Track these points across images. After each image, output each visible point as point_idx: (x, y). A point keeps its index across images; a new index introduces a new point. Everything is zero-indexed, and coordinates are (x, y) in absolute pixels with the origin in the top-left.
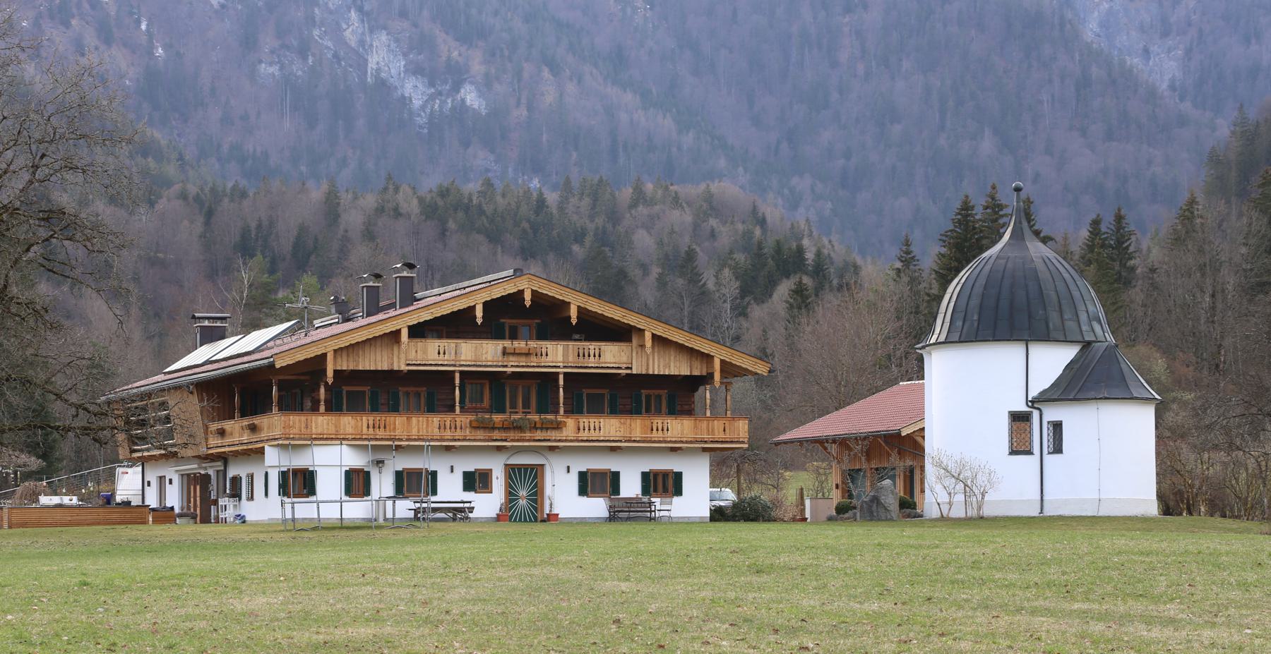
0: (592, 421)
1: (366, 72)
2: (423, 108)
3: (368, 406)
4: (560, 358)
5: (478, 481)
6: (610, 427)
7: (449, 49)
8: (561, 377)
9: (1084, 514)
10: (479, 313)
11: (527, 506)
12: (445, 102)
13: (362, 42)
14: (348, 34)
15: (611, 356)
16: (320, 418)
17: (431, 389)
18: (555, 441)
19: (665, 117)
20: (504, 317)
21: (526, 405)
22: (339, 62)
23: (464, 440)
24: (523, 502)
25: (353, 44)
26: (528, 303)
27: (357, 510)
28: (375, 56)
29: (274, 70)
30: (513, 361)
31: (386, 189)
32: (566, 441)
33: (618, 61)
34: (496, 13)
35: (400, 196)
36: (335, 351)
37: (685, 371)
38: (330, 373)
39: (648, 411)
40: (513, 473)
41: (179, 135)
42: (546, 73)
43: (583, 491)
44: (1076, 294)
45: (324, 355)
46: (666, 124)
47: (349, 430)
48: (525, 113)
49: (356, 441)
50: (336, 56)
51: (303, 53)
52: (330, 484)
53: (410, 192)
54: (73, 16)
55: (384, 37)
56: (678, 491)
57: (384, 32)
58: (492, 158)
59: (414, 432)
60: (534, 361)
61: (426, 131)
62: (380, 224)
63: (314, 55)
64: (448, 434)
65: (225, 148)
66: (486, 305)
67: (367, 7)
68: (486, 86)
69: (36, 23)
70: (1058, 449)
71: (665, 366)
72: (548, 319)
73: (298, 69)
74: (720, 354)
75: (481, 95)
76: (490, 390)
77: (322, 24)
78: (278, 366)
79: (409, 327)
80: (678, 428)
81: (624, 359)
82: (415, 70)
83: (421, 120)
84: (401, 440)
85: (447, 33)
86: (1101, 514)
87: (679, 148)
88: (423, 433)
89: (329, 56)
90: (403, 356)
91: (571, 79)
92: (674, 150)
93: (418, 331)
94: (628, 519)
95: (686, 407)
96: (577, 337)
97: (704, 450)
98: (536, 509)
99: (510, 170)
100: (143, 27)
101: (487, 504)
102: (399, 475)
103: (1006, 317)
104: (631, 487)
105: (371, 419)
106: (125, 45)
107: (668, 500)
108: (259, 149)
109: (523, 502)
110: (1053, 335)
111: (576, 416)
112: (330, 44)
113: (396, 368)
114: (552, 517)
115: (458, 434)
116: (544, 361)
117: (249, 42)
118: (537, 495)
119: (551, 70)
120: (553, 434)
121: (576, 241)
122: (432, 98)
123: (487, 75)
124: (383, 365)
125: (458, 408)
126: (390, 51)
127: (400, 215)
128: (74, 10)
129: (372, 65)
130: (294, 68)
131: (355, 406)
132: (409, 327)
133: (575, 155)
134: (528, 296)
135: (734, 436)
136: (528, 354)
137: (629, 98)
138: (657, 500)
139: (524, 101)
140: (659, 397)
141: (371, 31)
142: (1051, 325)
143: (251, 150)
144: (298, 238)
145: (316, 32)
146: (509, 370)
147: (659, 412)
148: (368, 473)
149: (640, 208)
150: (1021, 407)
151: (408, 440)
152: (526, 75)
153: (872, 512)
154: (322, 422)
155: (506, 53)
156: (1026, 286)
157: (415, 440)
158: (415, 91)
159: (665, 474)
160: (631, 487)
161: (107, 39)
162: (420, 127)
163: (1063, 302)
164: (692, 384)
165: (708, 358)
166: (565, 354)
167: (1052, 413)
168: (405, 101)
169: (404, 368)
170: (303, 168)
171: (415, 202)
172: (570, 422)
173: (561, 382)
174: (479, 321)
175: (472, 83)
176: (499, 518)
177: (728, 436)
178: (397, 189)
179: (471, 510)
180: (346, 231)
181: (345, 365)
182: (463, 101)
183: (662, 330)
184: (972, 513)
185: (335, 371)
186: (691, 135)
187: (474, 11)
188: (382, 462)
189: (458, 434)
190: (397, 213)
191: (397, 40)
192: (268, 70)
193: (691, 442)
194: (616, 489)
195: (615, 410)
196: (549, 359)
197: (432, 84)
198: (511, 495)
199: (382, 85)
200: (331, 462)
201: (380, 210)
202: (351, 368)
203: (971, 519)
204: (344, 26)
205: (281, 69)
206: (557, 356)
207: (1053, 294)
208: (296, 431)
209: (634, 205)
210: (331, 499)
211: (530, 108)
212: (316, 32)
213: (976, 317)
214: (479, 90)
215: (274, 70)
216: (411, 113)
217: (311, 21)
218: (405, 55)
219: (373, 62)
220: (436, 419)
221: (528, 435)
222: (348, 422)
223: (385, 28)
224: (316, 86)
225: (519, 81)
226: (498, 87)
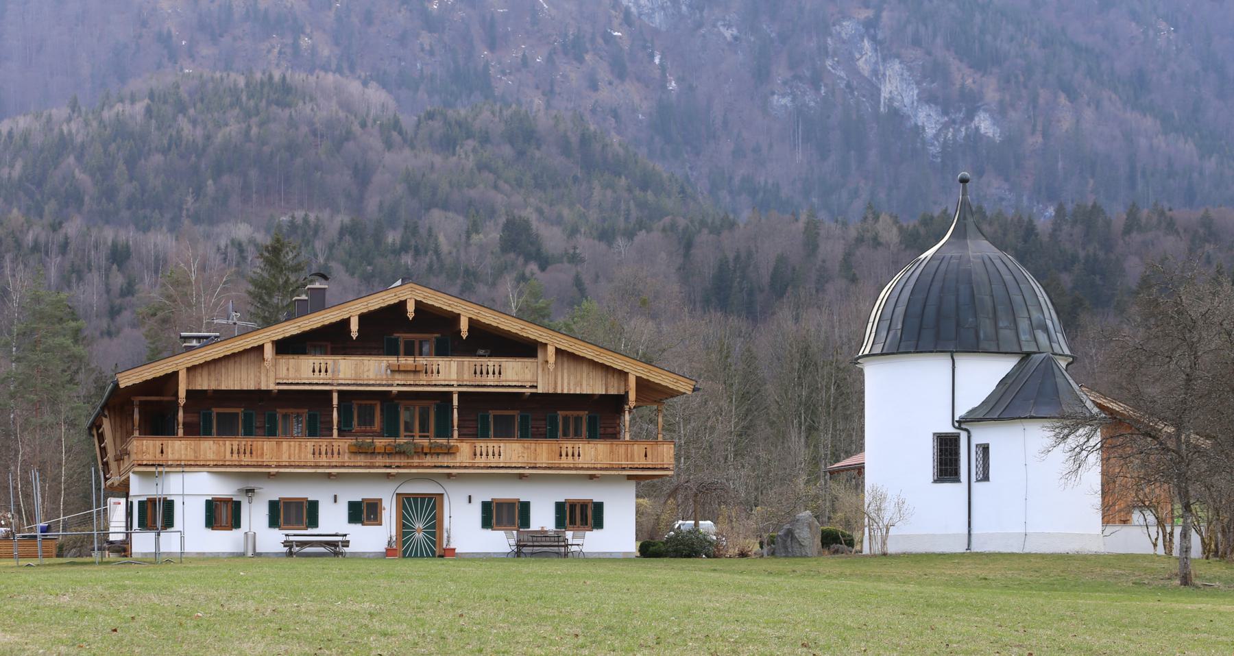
0: (490, 445)
1: (879, 102)
2: (936, 136)
3: (241, 430)
4: (454, 376)
5: (362, 513)
6: (513, 452)
7: (963, 76)
8: (455, 397)
9: (953, 551)
10: (354, 326)
11: (421, 535)
12: (959, 130)
13: (875, 72)
14: (861, 63)
15: (514, 374)
16: (177, 443)
17: (310, 410)
18: (448, 467)
19: (1186, 142)
20: (384, 331)
21: (424, 428)
22: (852, 92)
23: (343, 467)
24: (419, 535)
25: (866, 74)
26: (411, 315)
27: (224, 541)
28: (888, 85)
29: (786, 101)
30: (400, 379)
31: (865, 219)
32: (460, 467)
33: (1139, 83)
34: (1012, 39)
35: (880, 226)
36: (188, 369)
37: (599, 389)
38: (182, 394)
39: (566, 435)
40: (407, 503)
41: (691, 168)
42: (1063, 99)
43: (487, 523)
44: (1017, 298)
45: (176, 374)
46: (1187, 149)
47: (211, 456)
48: (1040, 140)
49: (219, 468)
50: (848, 85)
51: (815, 83)
52: (190, 515)
53: (890, 221)
54: (587, 52)
55: (897, 66)
56: (598, 524)
57: (897, 61)
58: (1006, 186)
59: (285, 458)
60: (423, 379)
61: (939, 160)
62: (858, 253)
63: (826, 86)
64: (324, 460)
65: (737, 181)
66: (363, 318)
67: (880, 36)
68: (1000, 113)
69: (550, 59)
70: (986, 478)
71: (575, 384)
72: (439, 333)
73: (811, 100)
74: (635, 370)
75: (995, 122)
76: (365, 412)
77: (835, 54)
78: (122, 386)
79: (273, 342)
80: (593, 453)
81: (528, 376)
82: (928, 98)
83: (935, 149)
84: (269, 466)
85: (961, 61)
86: (1026, 551)
87: (1201, 174)
88: (295, 459)
89: (842, 86)
90: (272, 374)
91: (1089, 105)
92: (1195, 175)
93: (286, 347)
94: (532, 554)
95: (610, 430)
96: (481, 352)
97: (630, 477)
98: (434, 543)
99: (1025, 198)
100: (657, 61)
101: (370, 539)
102: (274, 506)
103: (937, 326)
104: (543, 518)
105: (570, 447)
106: (638, 80)
107: (580, 533)
108: (770, 181)
109: (419, 535)
110: (984, 345)
111: (473, 440)
112: (842, 74)
113: (263, 387)
114: (449, 553)
115: (335, 460)
116: (435, 379)
117: (762, 74)
118: (435, 527)
119: (1068, 96)
120: (445, 460)
121: (1065, 269)
122: (946, 126)
123: (1001, 102)
124: (250, 385)
125: (335, 432)
126: (902, 80)
127: (879, 244)
128: (588, 46)
129: (885, 94)
130: (807, 99)
131: (227, 428)
132: (273, 342)
133: (1091, 182)
134: (411, 308)
135: (657, 462)
136: (415, 372)
137: (1149, 122)
138: (569, 534)
139: (1039, 128)
140: (578, 420)
141: (884, 60)
142: (982, 336)
143: (762, 183)
144: (776, 269)
145: (829, 63)
146: (395, 389)
147: (577, 435)
148: (238, 504)
149: (1134, 234)
150: (948, 428)
151: (277, 466)
152: (1041, 101)
153: (786, 548)
154: (178, 447)
155: (1021, 79)
156: (957, 290)
157: (285, 466)
158: (928, 120)
159: (584, 505)
160: (543, 518)
161: (619, 71)
162: (934, 156)
163: (999, 308)
164: (615, 404)
165: (623, 375)
166: (460, 372)
167: (981, 435)
168: (918, 130)
169: (272, 387)
170: (815, 200)
171: (895, 230)
172: (465, 448)
173: (455, 403)
174: (354, 335)
175: (985, 111)
176: (390, 552)
177: (649, 462)
178: (876, 218)
179: (346, 544)
180: (824, 261)
181: (204, 383)
182: (977, 129)
183: (567, 344)
184: (877, 548)
185: (188, 391)
186: (1213, 159)
187: (989, 38)
188: (252, 491)
189: (335, 460)
190: (876, 243)
191: (910, 69)
192: (780, 102)
193: (606, 469)
194: (525, 522)
195: (527, 433)
196: (441, 376)
197: (945, 112)
198: (404, 527)
199: (895, 115)
200: (192, 490)
201: (860, 240)
202: (213, 387)
203: (875, 556)
204: (857, 56)
205: (793, 100)
206: (451, 373)
207: (987, 299)
208: (149, 457)
209: (1128, 230)
210: (191, 534)
211: (1045, 135)
212: (829, 63)
213: (900, 326)
214: (992, 117)
215: (786, 101)
216: (924, 143)
217: (824, 51)
218: (918, 83)
219: (886, 90)
220: (310, 444)
221: (416, 461)
222: (209, 447)
223: (898, 56)
224: (829, 117)
225: (1034, 107)
226: (1013, 115)
